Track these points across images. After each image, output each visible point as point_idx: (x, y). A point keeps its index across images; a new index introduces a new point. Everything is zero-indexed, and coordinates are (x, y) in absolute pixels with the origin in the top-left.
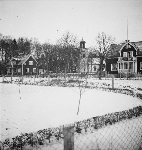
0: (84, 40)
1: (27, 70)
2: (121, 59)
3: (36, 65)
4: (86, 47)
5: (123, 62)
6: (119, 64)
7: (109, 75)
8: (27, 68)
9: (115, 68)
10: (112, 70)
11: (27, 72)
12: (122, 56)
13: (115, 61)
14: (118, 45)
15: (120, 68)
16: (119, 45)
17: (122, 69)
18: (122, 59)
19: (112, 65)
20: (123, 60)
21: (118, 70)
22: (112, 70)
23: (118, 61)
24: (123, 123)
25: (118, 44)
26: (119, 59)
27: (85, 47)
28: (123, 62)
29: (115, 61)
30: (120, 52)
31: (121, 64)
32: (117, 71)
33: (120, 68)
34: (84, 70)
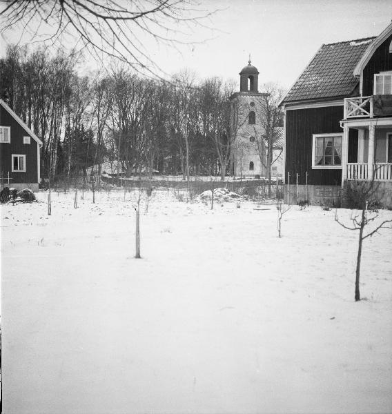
0: (253, 64)
1: (72, 164)
2: (359, 107)
3: (26, 140)
4: (261, 90)
5: (371, 124)
6: (353, 133)
7: (300, 189)
8: (18, 156)
9: (330, 154)
10: (314, 166)
11: (16, 167)
12: (368, 90)
13: (330, 120)
14: (353, 44)
15: (353, 157)
16: (359, 44)
17: (366, 160)
18: (367, 108)
19: (317, 141)
20: (371, 114)
21: (345, 165)
22: (314, 166)
23: (345, 118)
24: (364, 301)
25: (357, 41)
26: (351, 107)
27: (258, 92)
28: (371, 124)
29: (330, 120)
30: (358, 71)
31: (361, 134)
32: (340, 171)
33: (353, 157)
34: (252, 166)
